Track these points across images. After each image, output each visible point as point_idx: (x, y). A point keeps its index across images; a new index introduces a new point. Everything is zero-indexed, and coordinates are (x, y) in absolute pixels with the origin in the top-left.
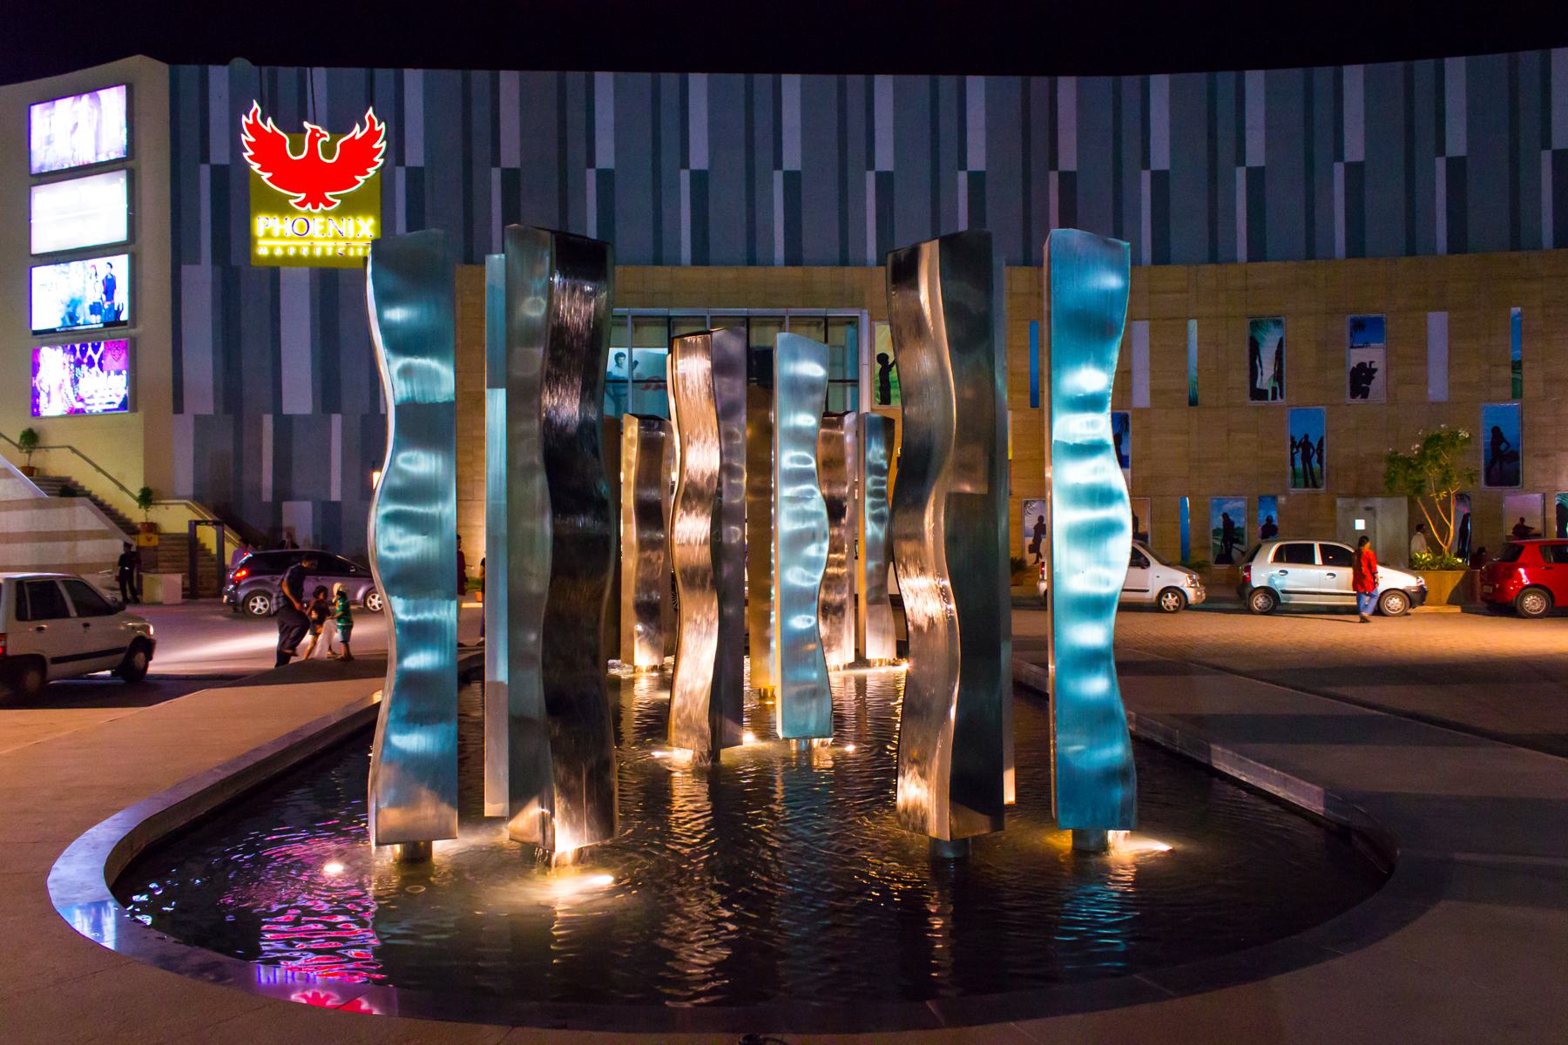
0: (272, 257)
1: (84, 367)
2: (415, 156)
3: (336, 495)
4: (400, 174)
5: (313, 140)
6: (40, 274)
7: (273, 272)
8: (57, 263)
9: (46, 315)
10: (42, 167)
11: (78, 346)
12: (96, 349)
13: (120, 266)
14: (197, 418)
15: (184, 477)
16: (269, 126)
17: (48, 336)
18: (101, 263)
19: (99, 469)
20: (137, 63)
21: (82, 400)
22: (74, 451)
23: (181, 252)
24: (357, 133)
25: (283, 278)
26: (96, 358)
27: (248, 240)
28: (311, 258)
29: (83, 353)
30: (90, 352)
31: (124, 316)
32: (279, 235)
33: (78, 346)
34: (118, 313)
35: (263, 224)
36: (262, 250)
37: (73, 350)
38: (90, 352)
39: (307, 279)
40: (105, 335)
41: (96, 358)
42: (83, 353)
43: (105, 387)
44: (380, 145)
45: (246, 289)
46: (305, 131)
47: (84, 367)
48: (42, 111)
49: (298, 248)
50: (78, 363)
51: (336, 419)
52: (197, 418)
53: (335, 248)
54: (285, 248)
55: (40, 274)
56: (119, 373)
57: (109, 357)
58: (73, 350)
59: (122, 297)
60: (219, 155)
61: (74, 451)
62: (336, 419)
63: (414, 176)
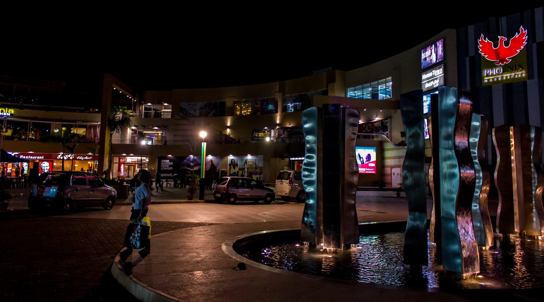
4: (534, 46)
5: (501, 41)
7: (490, 87)
24: (517, 36)
25: (493, 89)
27: (481, 78)
32: (491, 75)
44: (525, 38)
54: (493, 79)
60: (472, 53)
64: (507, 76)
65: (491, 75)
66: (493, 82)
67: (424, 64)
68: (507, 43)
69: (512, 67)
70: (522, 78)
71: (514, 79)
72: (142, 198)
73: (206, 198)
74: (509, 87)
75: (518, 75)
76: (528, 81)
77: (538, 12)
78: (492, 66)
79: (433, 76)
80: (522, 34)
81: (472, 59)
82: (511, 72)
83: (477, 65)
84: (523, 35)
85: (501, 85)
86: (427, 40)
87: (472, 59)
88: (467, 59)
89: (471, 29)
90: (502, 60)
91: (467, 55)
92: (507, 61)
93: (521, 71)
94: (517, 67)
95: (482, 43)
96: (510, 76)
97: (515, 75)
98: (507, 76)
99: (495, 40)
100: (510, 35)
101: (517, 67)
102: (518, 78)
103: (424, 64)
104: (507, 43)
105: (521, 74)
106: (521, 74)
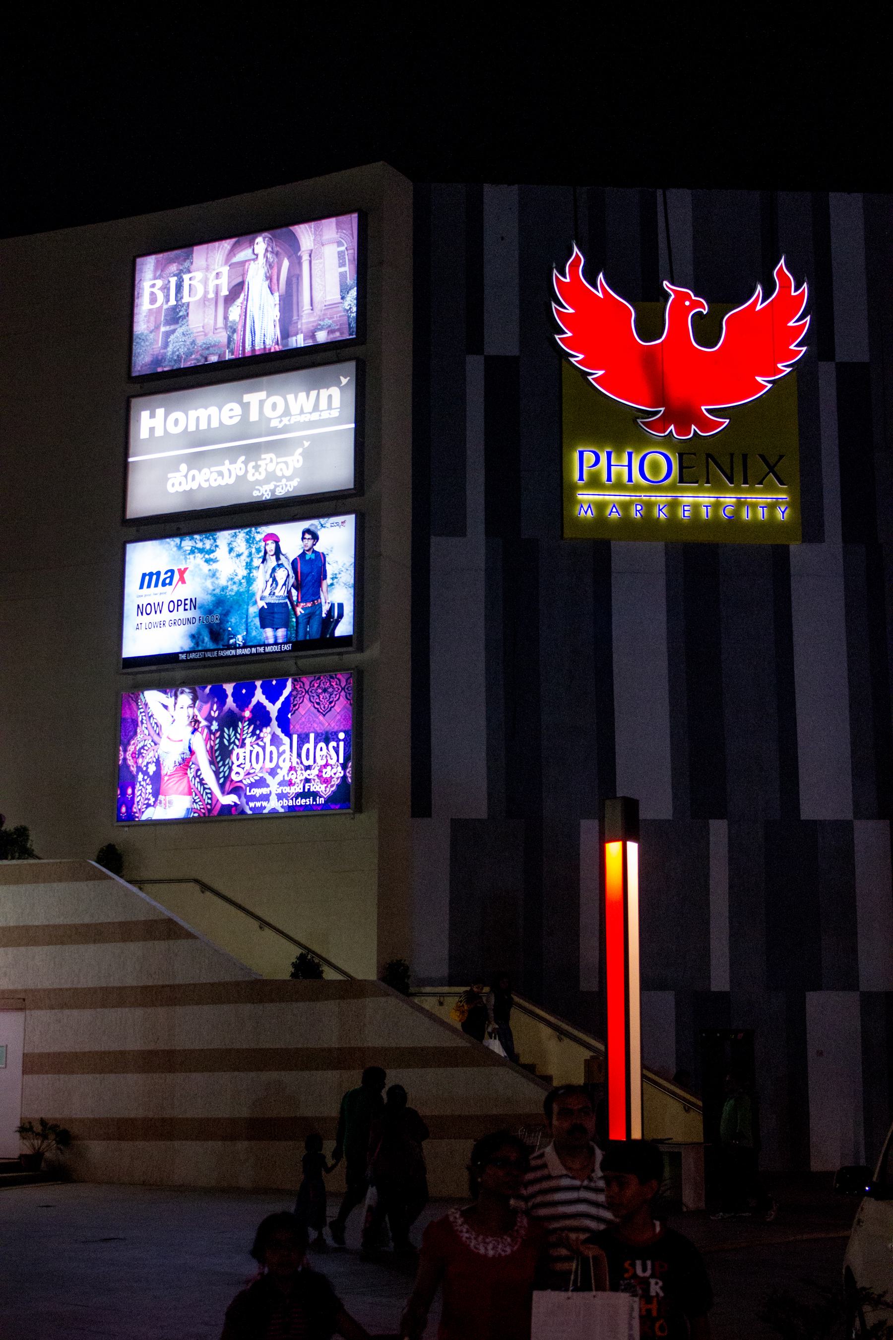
0: (601, 521)
1: (245, 728)
2: (853, 344)
3: (720, 980)
4: (827, 372)
5: (679, 311)
6: (144, 557)
7: (599, 547)
8: (180, 534)
9: (152, 629)
10: (157, 361)
11: (229, 688)
12: (272, 694)
13: (337, 539)
14: (459, 827)
15: (431, 952)
16: (601, 288)
17: (162, 670)
18: (290, 537)
19: (264, 924)
20: (375, 175)
21: (236, 790)
22: (205, 887)
23: (431, 514)
24: (757, 300)
25: (617, 563)
26: (273, 709)
27: (559, 492)
28: (673, 520)
29: (242, 700)
30: (259, 696)
31: (344, 628)
32: (616, 483)
33: (229, 688)
34: (331, 621)
35: (584, 460)
36: (586, 501)
37: (219, 696)
38: (259, 696)
39: (660, 563)
40: (290, 665)
41: (273, 709)
42: (242, 700)
43: (291, 766)
44: (800, 322)
45: (549, 575)
46: (667, 296)
47: (245, 728)
48: (160, 269)
49: (649, 506)
50: (230, 720)
51: (719, 831)
52: (459, 827)
53: (673, 505)
54: (626, 506)
55: (144, 557)
56: (326, 737)
57: (305, 707)
58: (219, 696)
59: (339, 592)
60: (502, 337)
61: (205, 887)
62: (719, 831)
63: (848, 374)
64: (699, 502)
65: (616, 483)
66: (626, 523)
67: (143, 358)
68: (707, 330)
69: (725, 461)
70: (770, 525)
71: (734, 521)
72: (194, 472)
73: (298, 272)
74: (699, 560)
75: (754, 506)
76: (795, 547)
77: (847, 213)
78: (621, 431)
79: (244, 428)
80: (782, 301)
81: (500, 371)
82: (718, 487)
83: (535, 415)
84: (788, 306)
85: (661, 545)
86: (240, 192)
87: (500, 371)
88: (475, 366)
89: (501, 207)
90: (683, 416)
91: (475, 345)
92: (705, 425)
93: (770, 489)
94: (757, 465)
95: (574, 293)
96: (716, 506)
97: (740, 504)
98: (699, 502)
99: (647, 295)
100: (724, 290)
101: (757, 465)
102: (756, 527)
103: (143, 358)
104: (707, 330)
105: (766, 505)
106: (766, 505)
